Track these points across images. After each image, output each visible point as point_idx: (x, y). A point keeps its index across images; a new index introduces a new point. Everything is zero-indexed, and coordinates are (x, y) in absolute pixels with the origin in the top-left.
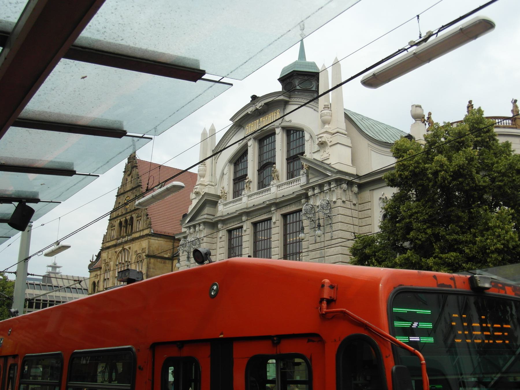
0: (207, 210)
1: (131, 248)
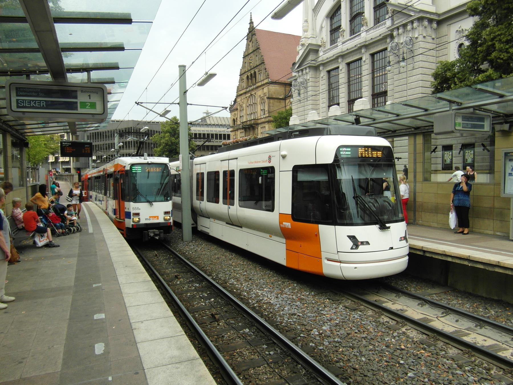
0: (311, 57)
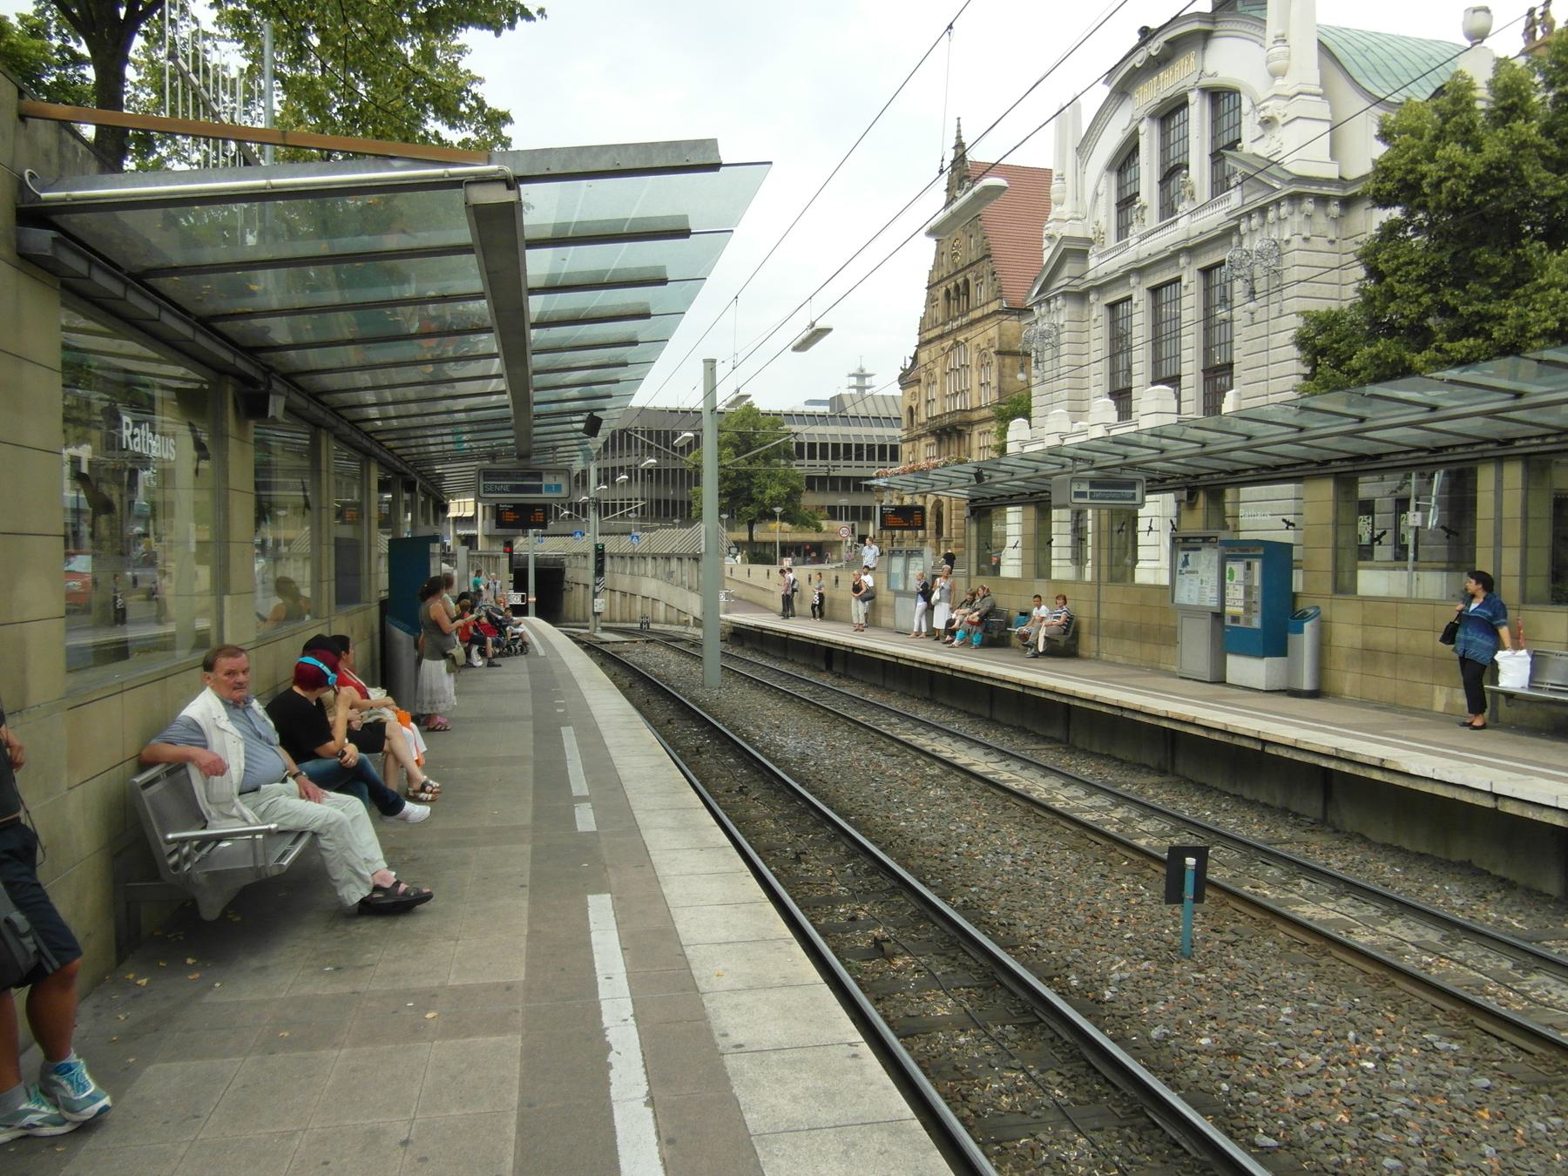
0: (1069, 269)
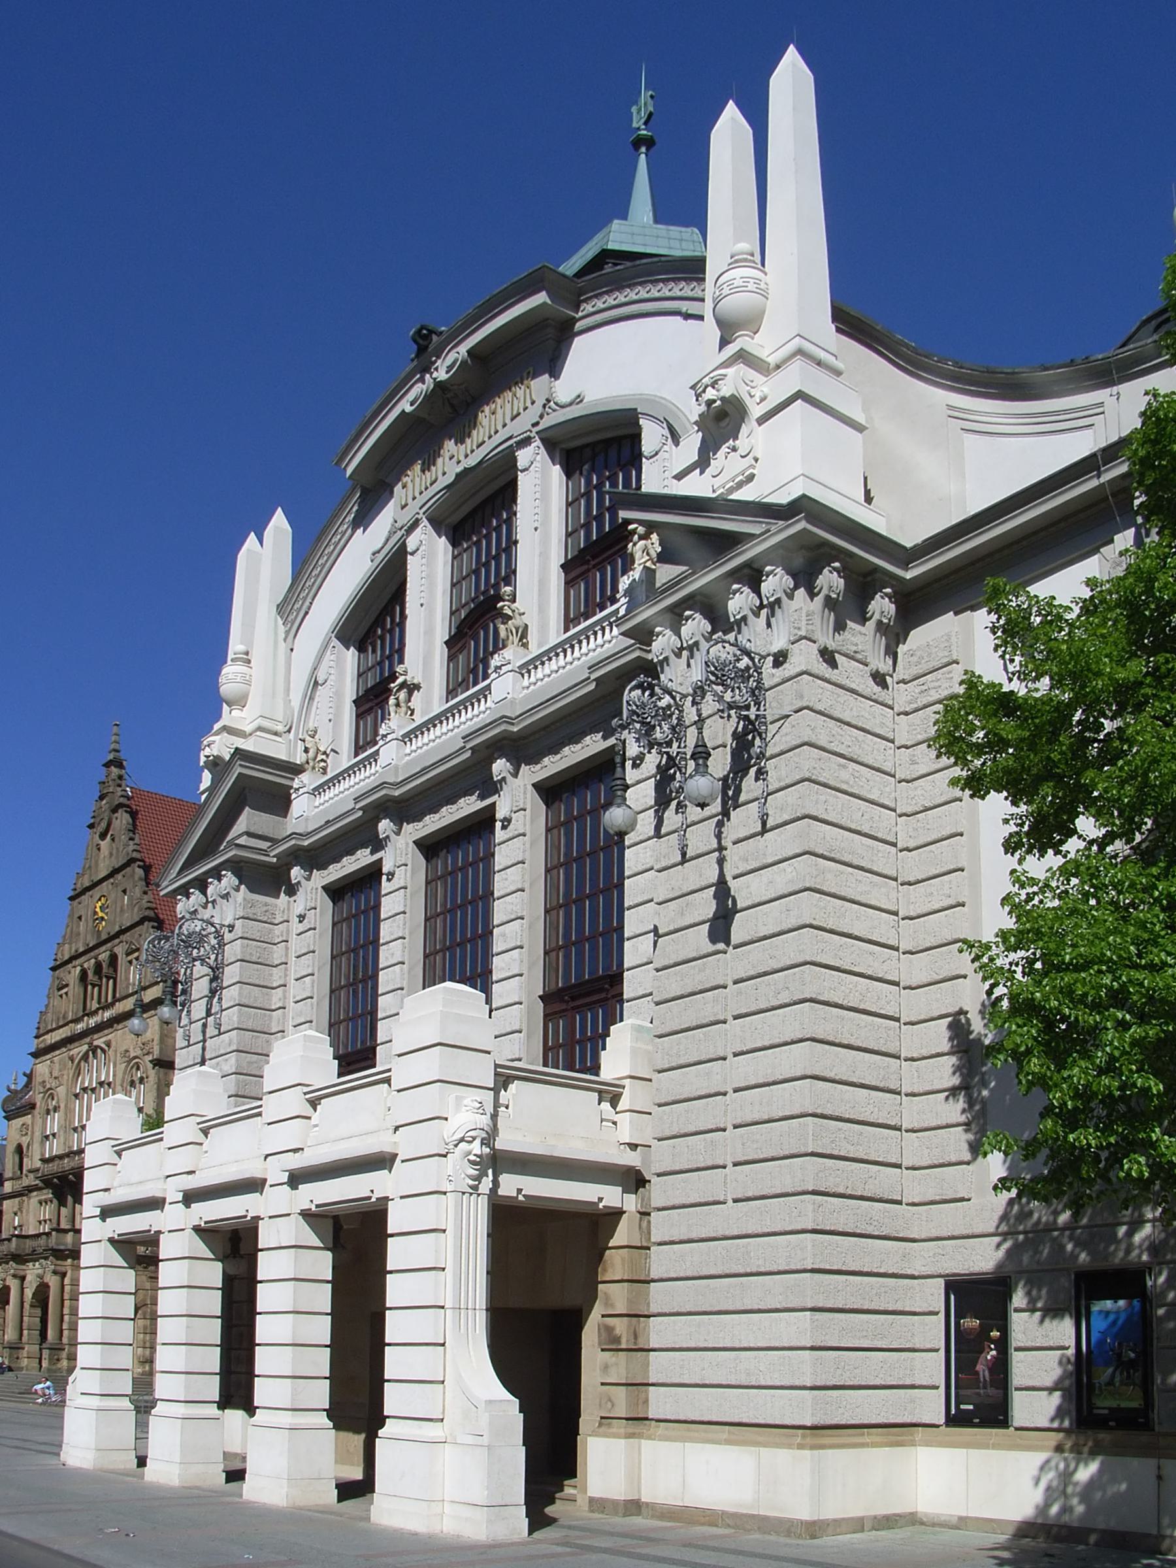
1: (113, 1044)
